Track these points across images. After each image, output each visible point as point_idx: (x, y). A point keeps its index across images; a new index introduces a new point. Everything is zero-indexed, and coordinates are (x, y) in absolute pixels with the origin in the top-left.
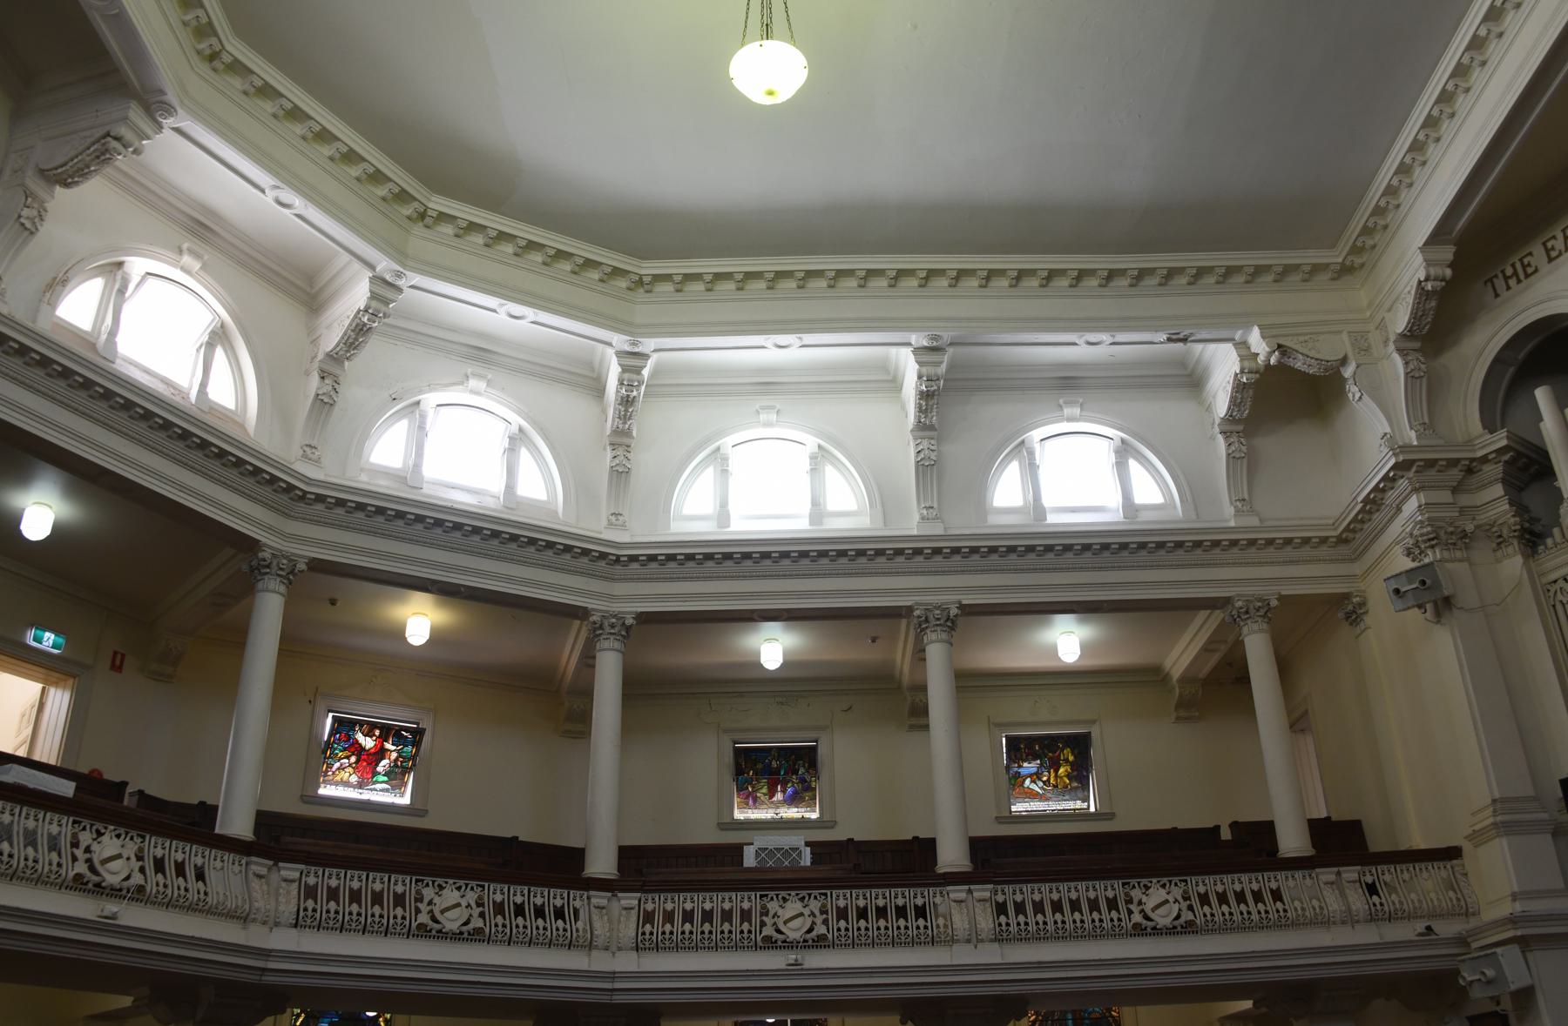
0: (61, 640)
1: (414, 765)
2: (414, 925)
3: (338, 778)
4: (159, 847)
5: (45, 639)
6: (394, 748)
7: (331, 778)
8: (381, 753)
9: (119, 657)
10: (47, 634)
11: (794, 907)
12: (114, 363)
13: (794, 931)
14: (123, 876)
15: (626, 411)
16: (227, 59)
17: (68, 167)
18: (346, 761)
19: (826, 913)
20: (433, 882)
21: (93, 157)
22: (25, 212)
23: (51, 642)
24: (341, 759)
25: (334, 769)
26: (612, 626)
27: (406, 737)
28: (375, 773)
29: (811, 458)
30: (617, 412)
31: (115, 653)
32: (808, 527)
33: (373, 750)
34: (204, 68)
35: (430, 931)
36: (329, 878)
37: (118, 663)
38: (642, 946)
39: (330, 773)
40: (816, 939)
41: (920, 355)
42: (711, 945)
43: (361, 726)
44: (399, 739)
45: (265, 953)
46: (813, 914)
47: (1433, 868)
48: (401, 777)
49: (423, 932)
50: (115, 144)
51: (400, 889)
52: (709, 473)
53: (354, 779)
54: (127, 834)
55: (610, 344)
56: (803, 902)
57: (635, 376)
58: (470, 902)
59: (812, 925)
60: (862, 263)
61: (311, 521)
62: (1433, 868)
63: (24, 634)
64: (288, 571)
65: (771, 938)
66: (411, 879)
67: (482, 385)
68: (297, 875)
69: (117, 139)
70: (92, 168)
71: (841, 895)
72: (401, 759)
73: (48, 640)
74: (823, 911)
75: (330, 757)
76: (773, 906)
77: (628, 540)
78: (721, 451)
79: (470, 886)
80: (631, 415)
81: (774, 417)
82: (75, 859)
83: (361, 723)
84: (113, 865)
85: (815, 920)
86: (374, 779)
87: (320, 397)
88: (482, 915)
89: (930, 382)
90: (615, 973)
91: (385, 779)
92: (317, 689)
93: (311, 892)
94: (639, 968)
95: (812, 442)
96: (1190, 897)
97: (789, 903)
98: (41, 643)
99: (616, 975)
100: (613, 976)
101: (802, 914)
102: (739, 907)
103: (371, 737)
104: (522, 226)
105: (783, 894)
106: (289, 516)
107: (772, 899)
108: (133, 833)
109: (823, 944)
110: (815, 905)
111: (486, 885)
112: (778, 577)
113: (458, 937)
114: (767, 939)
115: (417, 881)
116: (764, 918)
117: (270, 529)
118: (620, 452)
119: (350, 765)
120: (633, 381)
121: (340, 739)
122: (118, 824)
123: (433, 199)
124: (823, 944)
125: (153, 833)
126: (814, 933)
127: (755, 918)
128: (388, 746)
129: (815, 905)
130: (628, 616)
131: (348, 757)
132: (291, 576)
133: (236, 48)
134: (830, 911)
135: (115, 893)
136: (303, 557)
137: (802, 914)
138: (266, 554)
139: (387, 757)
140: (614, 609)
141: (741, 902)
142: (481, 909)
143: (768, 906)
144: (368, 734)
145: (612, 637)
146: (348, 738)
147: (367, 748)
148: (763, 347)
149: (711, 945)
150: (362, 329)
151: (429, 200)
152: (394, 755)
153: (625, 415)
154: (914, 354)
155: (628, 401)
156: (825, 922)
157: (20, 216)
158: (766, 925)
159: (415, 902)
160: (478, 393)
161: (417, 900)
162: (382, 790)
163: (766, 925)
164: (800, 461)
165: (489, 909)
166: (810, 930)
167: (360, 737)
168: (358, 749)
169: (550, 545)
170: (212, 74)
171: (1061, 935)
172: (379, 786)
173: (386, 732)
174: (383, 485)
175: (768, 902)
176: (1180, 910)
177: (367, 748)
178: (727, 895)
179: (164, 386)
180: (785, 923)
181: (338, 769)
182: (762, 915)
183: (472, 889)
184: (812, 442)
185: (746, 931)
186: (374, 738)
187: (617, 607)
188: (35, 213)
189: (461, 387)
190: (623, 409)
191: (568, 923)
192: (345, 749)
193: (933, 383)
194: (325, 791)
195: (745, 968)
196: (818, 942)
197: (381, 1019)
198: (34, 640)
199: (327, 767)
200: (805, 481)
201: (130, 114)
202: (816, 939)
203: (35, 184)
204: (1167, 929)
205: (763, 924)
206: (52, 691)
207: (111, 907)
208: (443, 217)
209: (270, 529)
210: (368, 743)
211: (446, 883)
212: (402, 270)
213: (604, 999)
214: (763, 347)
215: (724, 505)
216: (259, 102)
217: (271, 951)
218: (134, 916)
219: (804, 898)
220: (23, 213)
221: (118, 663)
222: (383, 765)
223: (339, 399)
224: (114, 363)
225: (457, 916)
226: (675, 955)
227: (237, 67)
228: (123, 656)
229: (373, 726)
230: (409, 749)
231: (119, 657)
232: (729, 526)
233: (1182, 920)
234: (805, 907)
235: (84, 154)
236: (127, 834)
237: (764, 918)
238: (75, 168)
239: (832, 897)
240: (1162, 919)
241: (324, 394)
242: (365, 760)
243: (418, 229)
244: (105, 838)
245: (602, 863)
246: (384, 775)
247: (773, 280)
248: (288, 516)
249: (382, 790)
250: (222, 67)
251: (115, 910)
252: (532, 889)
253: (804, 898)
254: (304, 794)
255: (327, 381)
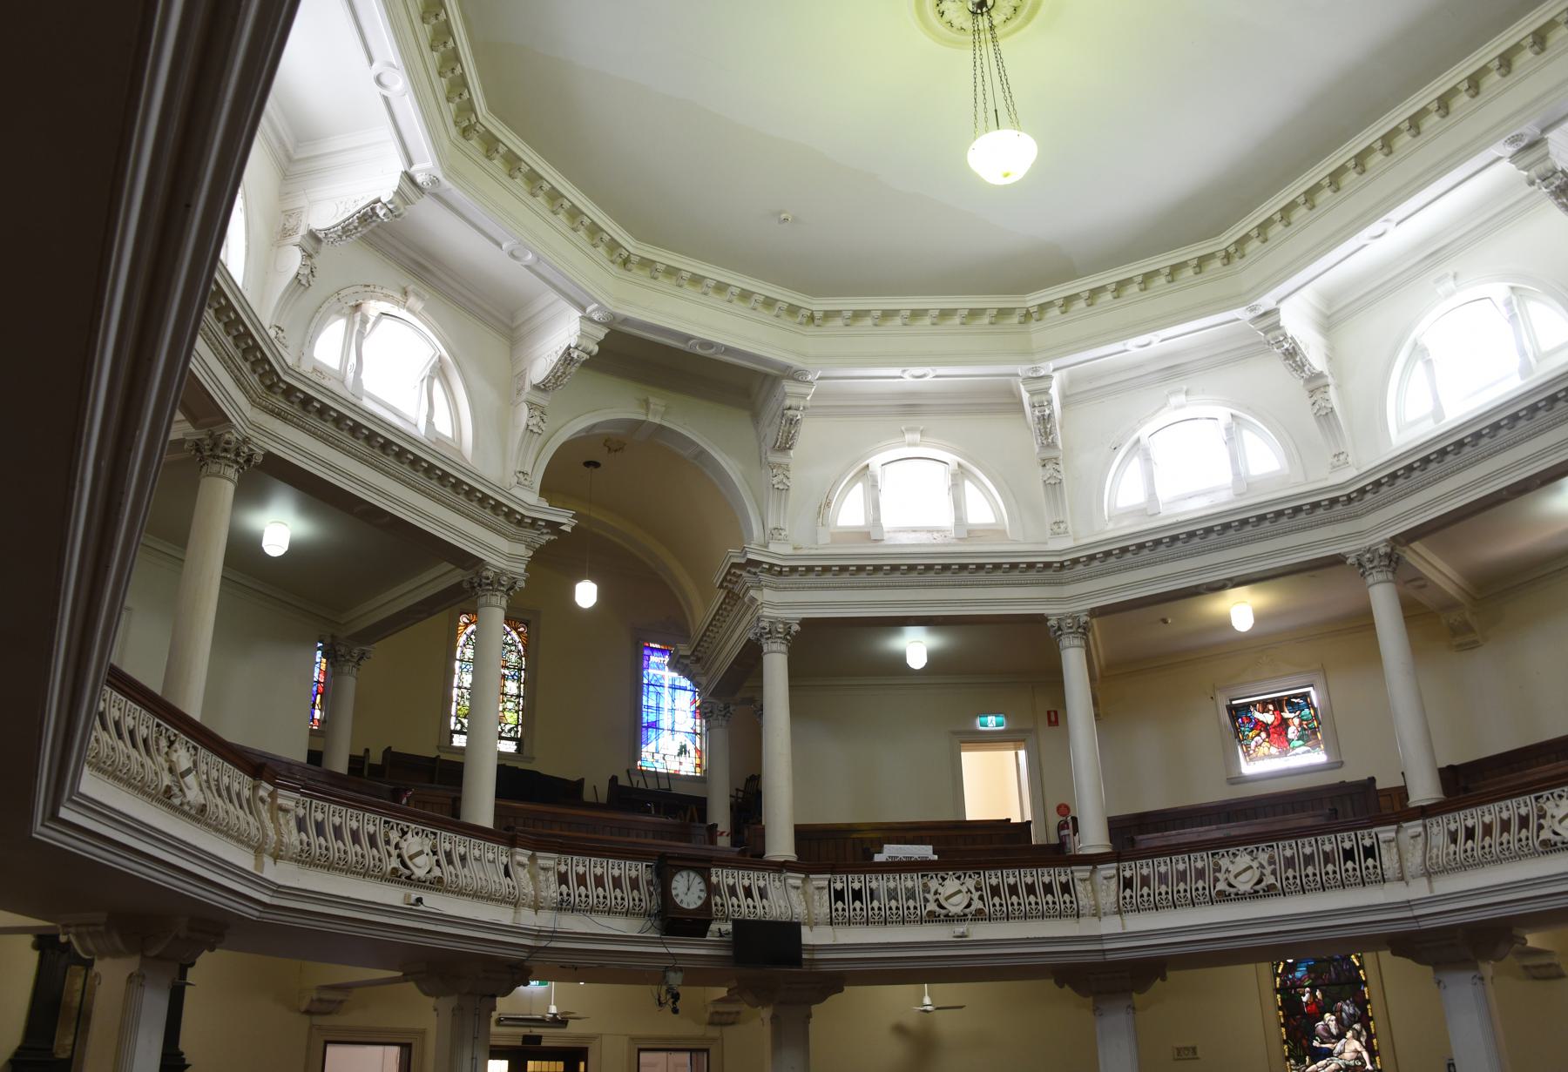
0: (1001, 719)
1: (1319, 723)
2: (924, 913)
3: (1260, 754)
4: (1011, 876)
5: (989, 722)
6: (1292, 715)
7: (1254, 755)
8: (1284, 724)
9: (1052, 714)
10: (990, 718)
11: (1244, 860)
12: (883, 540)
13: (1244, 884)
14: (965, 903)
15: (1295, 362)
16: (820, 315)
17: (780, 440)
18: (1257, 738)
19: (1275, 863)
20: (1227, 852)
21: (788, 425)
22: (775, 480)
23: (994, 722)
24: (1253, 739)
25: (1253, 747)
26: (1371, 561)
27: (1298, 703)
28: (1289, 741)
29: (1226, 429)
30: (1289, 367)
31: (1049, 713)
32: (1523, 382)
33: (1276, 723)
34: (811, 329)
35: (1230, 895)
36: (1141, 868)
37: (1053, 718)
38: (1503, 857)
39: (1251, 752)
40: (1266, 889)
41: (1519, 160)
42: (1317, 886)
43: (1255, 706)
44: (1294, 707)
45: (1099, 939)
46: (1262, 866)
47: (883, 879)
48: (1314, 737)
49: (1223, 897)
50: (790, 413)
51: (1199, 865)
52: (1420, 365)
53: (1274, 750)
54: (965, 874)
55: (1017, 375)
56: (1252, 856)
57: (1277, 333)
58: (1262, 862)
59: (1261, 876)
60: (1399, 115)
61: (1079, 581)
62: (883, 879)
63: (974, 723)
64: (1076, 626)
65: (1225, 892)
66: (1208, 854)
67: (1181, 398)
68: (1114, 872)
69: (790, 408)
70: (793, 432)
71: (1199, 857)
72: (1305, 723)
73: (992, 722)
74: (1271, 861)
75: (1243, 740)
76: (1224, 863)
77: (1355, 473)
78: (1419, 344)
79: (1260, 849)
80: (1302, 362)
81: (1450, 284)
82: (926, 900)
83: (1254, 704)
84: (954, 900)
85: (1264, 871)
86: (1291, 746)
87: (1047, 482)
88: (1274, 873)
89: (1547, 182)
90: (1409, 902)
91: (1301, 742)
92: (1214, 686)
93: (1128, 883)
94: (1431, 892)
95: (1223, 413)
96: (981, 887)
97: (1239, 857)
98: (987, 726)
99: (1412, 903)
100: (1408, 905)
101: (1251, 867)
102: (1193, 868)
103: (1268, 712)
104: (1078, 282)
105: (1232, 850)
106: (1062, 583)
107: (1223, 855)
108: (969, 873)
109: (1273, 893)
110: (1263, 857)
111: (1275, 844)
112: (1503, 449)
113: (1255, 895)
114: (1221, 893)
115: (1213, 855)
116: (1217, 874)
117: (1048, 601)
118: (1318, 396)
119: (1264, 741)
120: (1277, 338)
121: (1243, 723)
122: (954, 869)
123: (1028, 299)
124: (1273, 893)
125: (985, 869)
126: (1263, 884)
127: (1533, 824)
128: (1286, 715)
129: (1263, 857)
130: (1380, 546)
131: (1258, 735)
132: (1084, 631)
133: (819, 305)
134: (1277, 861)
135: (962, 918)
136: (1083, 611)
137: (1251, 867)
138: (1053, 622)
139: (1291, 724)
140: (1363, 546)
141: (1518, 808)
142: (980, 893)
143: (1220, 862)
144: (1265, 710)
145: (1374, 571)
146: (1250, 719)
147: (1270, 723)
148: (1364, 246)
149: (1317, 886)
150: (1044, 419)
151: (1025, 302)
152: (1296, 721)
153: (1046, 432)
154: (1513, 163)
155: (1290, 353)
156: (1274, 873)
157: (773, 485)
158: (1219, 880)
159: (1214, 872)
160: (1181, 406)
161: (1540, 817)
162: (1303, 753)
163: (1219, 880)
164: (1216, 433)
165: (987, 893)
166: (1260, 881)
167: (1258, 715)
168: (1264, 727)
169: (1244, 522)
170: (818, 329)
171: (999, 916)
172: (1298, 750)
173: (1279, 704)
174: (1128, 526)
175: (1544, 803)
176: (971, 899)
177: (1270, 723)
178: (1502, 804)
179: (929, 535)
180: (1236, 877)
181: (1256, 746)
182: (1215, 871)
183: (1263, 850)
184: (1223, 413)
185: (1291, 878)
186: (1271, 712)
187: (1367, 542)
188: (781, 477)
189: (1166, 409)
190: (1291, 362)
191: (1357, 863)
192: (1252, 730)
193: (1552, 180)
194: (1248, 768)
195: (1523, 878)
196: (1268, 891)
197: (1353, 957)
198: (981, 726)
199: (1247, 748)
200: (1224, 454)
201: (786, 390)
202: (1266, 889)
203: (775, 458)
204: (958, 916)
205: (1216, 880)
206: (1019, 752)
207: (960, 929)
208: (1043, 307)
209: (1048, 601)
210: (1268, 718)
211: (1238, 850)
212: (1034, 366)
213: (1412, 926)
214: (1364, 246)
215: (1436, 398)
216: (860, 324)
217: (1101, 936)
218: (981, 931)
219: (1252, 851)
220: (774, 482)
221: (1053, 718)
222: (1292, 732)
223: (1063, 476)
224: (883, 540)
225: (1248, 879)
226: (1463, 874)
227: (829, 315)
228: (1056, 713)
229: (1265, 703)
230: (1307, 711)
231: (1052, 714)
232: (1444, 418)
233: (973, 908)
234: (1253, 860)
235: (782, 428)
236: (965, 874)
237: (1217, 874)
238: (784, 438)
239: (1278, 847)
240: (954, 908)
241: (1049, 478)
242: (1274, 733)
243: (1033, 325)
244: (947, 882)
245: (1424, 790)
246: (1298, 740)
247: (1170, 274)
248: (1061, 584)
249: (1303, 753)
250: (820, 321)
251: (962, 930)
252: (1319, 838)
253: (1252, 851)
254: (1229, 777)
255: (1048, 467)
